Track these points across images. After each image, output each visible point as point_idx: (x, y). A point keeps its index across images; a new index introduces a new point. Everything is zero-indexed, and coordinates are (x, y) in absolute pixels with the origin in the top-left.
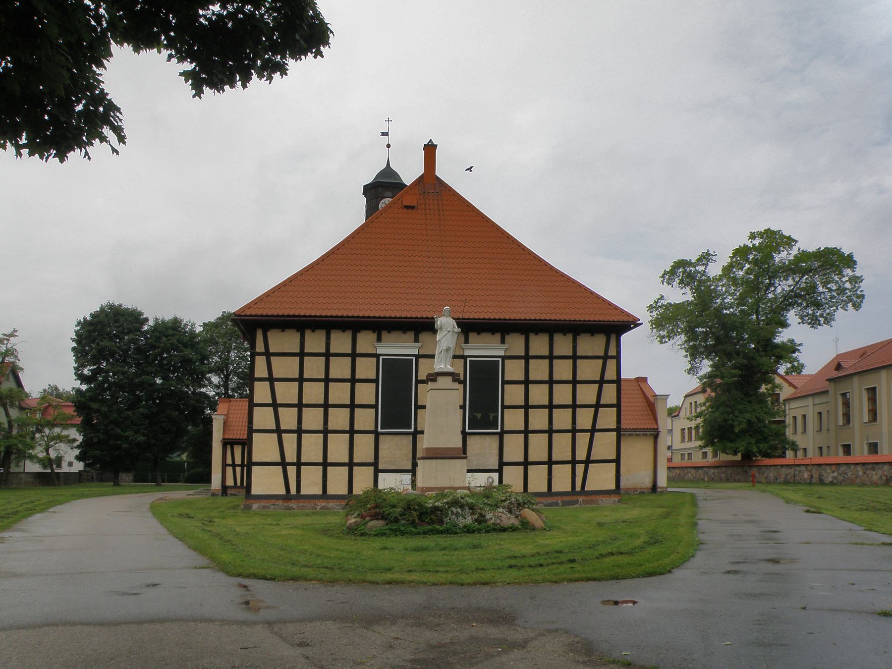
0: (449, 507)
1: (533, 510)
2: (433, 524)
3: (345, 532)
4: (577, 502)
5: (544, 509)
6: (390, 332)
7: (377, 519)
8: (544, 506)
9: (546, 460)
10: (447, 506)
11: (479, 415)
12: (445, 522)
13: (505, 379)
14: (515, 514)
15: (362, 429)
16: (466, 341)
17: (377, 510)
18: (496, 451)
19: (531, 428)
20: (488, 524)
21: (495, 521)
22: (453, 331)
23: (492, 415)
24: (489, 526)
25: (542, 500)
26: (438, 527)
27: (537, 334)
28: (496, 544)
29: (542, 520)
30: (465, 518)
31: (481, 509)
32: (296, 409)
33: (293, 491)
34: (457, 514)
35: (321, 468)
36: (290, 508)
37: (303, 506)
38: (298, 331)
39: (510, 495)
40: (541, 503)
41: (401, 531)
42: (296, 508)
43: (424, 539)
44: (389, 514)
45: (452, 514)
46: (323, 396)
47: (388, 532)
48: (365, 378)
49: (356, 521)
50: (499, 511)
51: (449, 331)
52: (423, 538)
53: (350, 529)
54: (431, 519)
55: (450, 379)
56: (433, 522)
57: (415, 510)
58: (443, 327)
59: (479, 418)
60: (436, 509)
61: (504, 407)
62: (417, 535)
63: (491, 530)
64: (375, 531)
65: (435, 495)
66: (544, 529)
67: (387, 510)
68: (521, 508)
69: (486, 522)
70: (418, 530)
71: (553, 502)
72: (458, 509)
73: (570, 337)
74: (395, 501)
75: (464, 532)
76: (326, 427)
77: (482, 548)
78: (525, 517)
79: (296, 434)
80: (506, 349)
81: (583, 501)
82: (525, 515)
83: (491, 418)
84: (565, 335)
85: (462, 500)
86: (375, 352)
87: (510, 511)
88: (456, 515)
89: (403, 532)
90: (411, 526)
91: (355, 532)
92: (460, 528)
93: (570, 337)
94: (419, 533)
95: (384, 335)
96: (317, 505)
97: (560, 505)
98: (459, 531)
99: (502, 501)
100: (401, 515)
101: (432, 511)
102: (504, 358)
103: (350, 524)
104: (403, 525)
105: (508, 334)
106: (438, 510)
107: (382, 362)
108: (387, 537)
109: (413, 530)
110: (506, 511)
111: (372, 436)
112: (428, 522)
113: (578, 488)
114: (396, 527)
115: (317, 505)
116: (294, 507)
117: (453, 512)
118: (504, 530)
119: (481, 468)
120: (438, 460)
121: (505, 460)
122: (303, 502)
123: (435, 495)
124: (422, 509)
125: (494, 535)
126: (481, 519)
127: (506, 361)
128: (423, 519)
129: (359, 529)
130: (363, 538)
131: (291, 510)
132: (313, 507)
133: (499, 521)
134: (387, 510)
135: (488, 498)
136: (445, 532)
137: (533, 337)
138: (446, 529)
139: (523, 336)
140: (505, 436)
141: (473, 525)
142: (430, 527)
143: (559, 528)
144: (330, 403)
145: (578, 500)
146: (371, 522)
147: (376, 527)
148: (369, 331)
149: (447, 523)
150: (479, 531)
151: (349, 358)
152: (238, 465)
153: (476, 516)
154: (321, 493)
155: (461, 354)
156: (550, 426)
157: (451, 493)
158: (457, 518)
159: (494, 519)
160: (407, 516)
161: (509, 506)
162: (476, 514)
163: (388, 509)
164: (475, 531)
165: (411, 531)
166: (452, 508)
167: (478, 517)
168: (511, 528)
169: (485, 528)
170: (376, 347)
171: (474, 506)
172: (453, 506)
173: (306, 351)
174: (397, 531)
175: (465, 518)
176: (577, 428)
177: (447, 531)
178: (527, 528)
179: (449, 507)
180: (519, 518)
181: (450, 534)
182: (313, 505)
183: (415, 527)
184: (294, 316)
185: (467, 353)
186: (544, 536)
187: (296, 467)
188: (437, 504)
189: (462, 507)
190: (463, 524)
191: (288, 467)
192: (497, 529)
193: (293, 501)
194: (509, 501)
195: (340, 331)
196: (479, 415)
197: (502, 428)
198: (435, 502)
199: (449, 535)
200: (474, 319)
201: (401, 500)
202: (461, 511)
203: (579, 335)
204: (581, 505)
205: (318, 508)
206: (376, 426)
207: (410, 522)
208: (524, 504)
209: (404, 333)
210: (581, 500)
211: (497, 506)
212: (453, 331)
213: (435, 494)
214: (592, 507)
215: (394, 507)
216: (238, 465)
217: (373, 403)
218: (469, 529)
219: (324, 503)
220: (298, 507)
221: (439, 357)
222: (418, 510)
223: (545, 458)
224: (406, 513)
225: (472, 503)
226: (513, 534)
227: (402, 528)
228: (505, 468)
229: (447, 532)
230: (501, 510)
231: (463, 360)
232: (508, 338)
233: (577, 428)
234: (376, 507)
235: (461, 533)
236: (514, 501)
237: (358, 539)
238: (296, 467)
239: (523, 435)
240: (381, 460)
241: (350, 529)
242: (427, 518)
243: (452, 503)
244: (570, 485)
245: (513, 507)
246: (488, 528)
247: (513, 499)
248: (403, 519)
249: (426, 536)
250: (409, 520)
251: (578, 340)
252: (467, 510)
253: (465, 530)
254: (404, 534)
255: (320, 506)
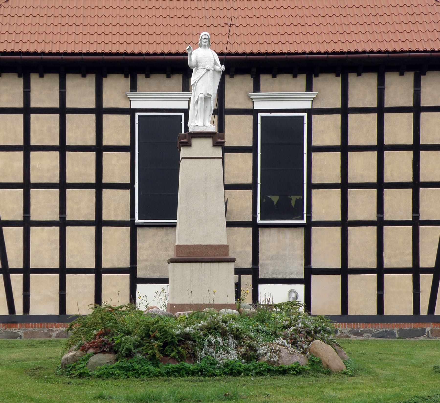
0: (205, 335)
1: (329, 343)
2: (181, 361)
3: (59, 372)
4: (422, 332)
5: (371, 340)
6: (233, 77)
7: (104, 352)
8: (372, 336)
9: (375, 266)
10: (202, 333)
11: (275, 199)
12: (199, 358)
13: (313, 145)
14: (302, 347)
15: (113, 219)
16: (257, 88)
17: (105, 338)
18: (300, 252)
19: (351, 217)
20: (261, 362)
21: (271, 357)
22: (214, 70)
23: (294, 199)
24: (262, 365)
25: (368, 327)
26: (187, 364)
27: (359, 75)
28: (260, 394)
29: (342, 358)
30: (228, 353)
31: (251, 338)
32: (21, 191)
33: (19, 310)
34: (216, 346)
35: (57, 276)
36: (15, 336)
37: (33, 332)
38: (19, 76)
39: (295, 318)
40: (366, 332)
41: (134, 370)
42: (23, 335)
43: (167, 383)
44: (120, 344)
45: (209, 346)
46: (58, 172)
47: (116, 371)
48: (115, 144)
49: (74, 355)
50: (277, 342)
51: (208, 70)
52: (165, 381)
53: (66, 367)
54: (179, 352)
55: (209, 142)
56: (182, 357)
57: (156, 339)
58: (199, 64)
59: (275, 203)
60: (187, 337)
61: (311, 186)
62: (157, 376)
63: (264, 371)
64: (100, 370)
65: (187, 316)
66: (345, 373)
67: (118, 338)
68: (310, 339)
69: (258, 359)
70: (159, 370)
71: (386, 331)
72: (218, 339)
73: (410, 77)
74: (130, 325)
75: (225, 373)
76: (28, 215)
77: (237, 399)
78: (316, 353)
79: (22, 228)
80: (314, 98)
81: (432, 330)
82: (316, 351)
83: (293, 203)
84: (402, 74)
85: (224, 325)
86: (128, 107)
87: (294, 343)
88: (215, 346)
89: (138, 372)
90: (149, 363)
91: (72, 372)
92: (219, 368)
93: (410, 77)
94: (159, 375)
95: (141, 80)
96: (52, 331)
97: (397, 336)
98: (217, 371)
99: (284, 327)
100: (136, 346)
101: (179, 341)
102: (310, 112)
103: (66, 359)
104: (138, 362)
105: (317, 76)
106: (189, 339)
107: (139, 122)
108: (116, 379)
109: (152, 369)
110: (288, 343)
111: (126, 230)
112: (174, 358)
113: (424, 310)
114: (129, 364)
115: (52, 331)
116: (20, 334)
117: (210, 342)
118: (284, 372)
119: (280, 277)
120: (194, 264)
121: (314, 265)
122: (32, 327)
123: (187, 316)
124: (166, 338)
125: (267, 380)
126: (251, 353)
127: (315, 118)
128: (167, 353)
129: (77, 367)
130: (81, 380)
131: (16, 338)
132: (46, 334)
133: (276, 359)
134: (117, 339)
135: (263, 321)
136: (197, 373)
137: (352, 79)
138: (199, 368)
139: (339, 79)
140: (314, 229)
141: (238, 363)
142: (177, 365)
143: (371, 373)
144: (68, 181)
145: (425, 330)
146: (95, 356)
147: (101, 364)
148: (120, 75)
149: (201, 359)
150: (247, 372)
151: (103, 117)
152: (16, 271)
153: (243, 350)
154: (57, 312)
155: (249, 107)
156: (415, 215)
157: (211, 314)
158: (217, 353)
159: (269, 354)
160: (144, 348)
161: (292, 335)
162: (243, 346)
163: (119, 336)
164: (242, 372)
165: (149, 370)
166: (210, 336)
167: (247, 350)
168: (294, 369)
169: (256, 368)
170: (252, 99)
171: (240, 334)
172: (211, 333)
173: (33, 105)
174: (129, 371)
175: (228, 353)
176: (421, 219)
177: (201, 371)
178: (319, 371)
179: (205, 335)
180: (308, 353)
181: (205, 376)
182: (46, 330)
183: (156, 365)
184: (12, 53)
185: (258, 106)
186: (341, 384)
187: (22, 275)
188: (187, 330)
189: (224, 334)
190: (225, 361)
191: (11, 275)
192: (273, 370)
193: (19, 325)
194: (293, 328)
195: (79, 76)
196: (275, 199)
197: (309, 218)
198: (185, 327)
199: (202, 378)
200: (267, 54)
201: (138, 323)
202: (223, 341)
203: (425, 74)
204: (428, 336)
205: (54, 334)
206: (132, 215)
207: (147, 356)
208: (315, 332)
209: (168, 77)
210: (428, 329)
211: (275, 334)
212: (214, 70)
213: (188, 314)
214: (415, 341)
215: (128, 333)
216: (16, 271)
217: (250, 181)
218: (232, 369)
219: (61, 327)
220: (25, 334)
221: (195, 109)
222: (160, 338)
223: (372, 263)
224: (144, 343)
225: (238, 329)
226: (295, 378)
227: (137, 366)
228: (314, 277)
229: (201, 372)
230: (280, 341)
231: (251, 117)
232: (317, 82)
233: (421, 219)
234: (106, 333)
235: (220, 375)
236: (301, 328)
237: (73, 381)
238: (22, 275)
239: (339, 229)
240: (140, 265)
241: (66, 367)
242: (173, 351)
243: (210, 329)
244: (411, 306)
245: (299, 337)
246: (260, 368)
247: (300, 325)
248: (139, 352)
249: (170, 378)
250: (147, 354)
251: (422, 83)
252: (231, 340)
253: (226, 370)
254: (139, 375)
255: (56, 332)
